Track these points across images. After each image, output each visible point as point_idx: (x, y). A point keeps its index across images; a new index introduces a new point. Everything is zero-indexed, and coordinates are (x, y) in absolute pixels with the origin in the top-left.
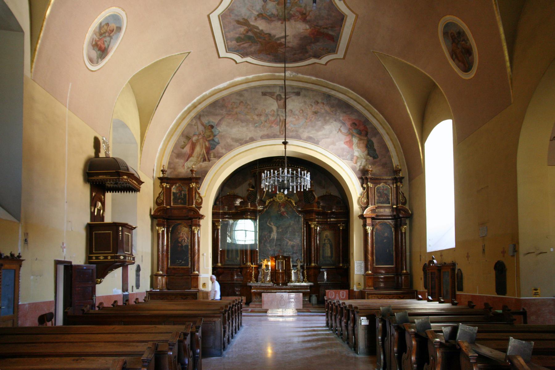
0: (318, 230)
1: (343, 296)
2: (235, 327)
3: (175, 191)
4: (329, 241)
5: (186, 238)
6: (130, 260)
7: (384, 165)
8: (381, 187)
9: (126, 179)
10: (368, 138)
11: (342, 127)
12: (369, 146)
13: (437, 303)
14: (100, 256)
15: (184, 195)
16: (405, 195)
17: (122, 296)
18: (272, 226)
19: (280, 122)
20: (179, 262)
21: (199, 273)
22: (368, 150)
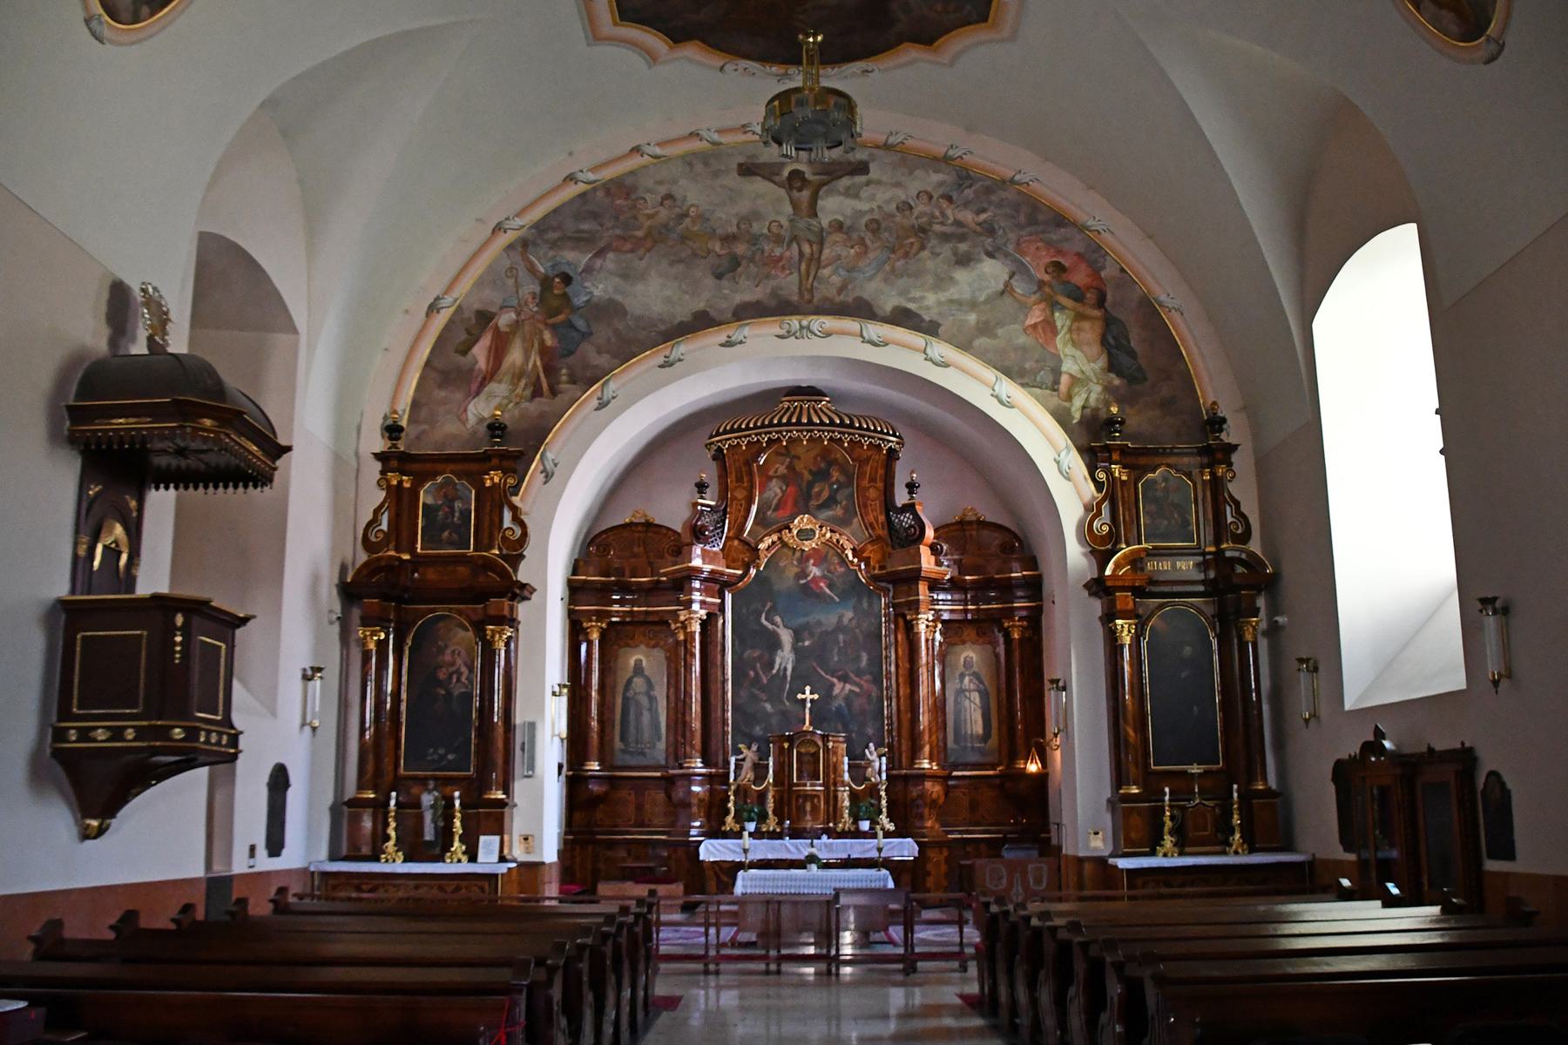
0: (937, 644)
1: (1038, 881)
2: (617, 1024)
3: (430, 501)
4: (975, 681)
5: (464, 669)
6: (219, 743)
7: (1166, 405)
8: (1160, 480)
9: (208, 431)
10: (1106, 310)
11: (1016, 277)
12: (1111, 341)
13: (1378, 908)
14: (98, 727)
15: (461, 512)
16: (1244, 509)
17: (203, 886)
18: (778, 627)
19: (800, 261)
20: (436, 757)
21: (508, 797)
22: (1110, 355)
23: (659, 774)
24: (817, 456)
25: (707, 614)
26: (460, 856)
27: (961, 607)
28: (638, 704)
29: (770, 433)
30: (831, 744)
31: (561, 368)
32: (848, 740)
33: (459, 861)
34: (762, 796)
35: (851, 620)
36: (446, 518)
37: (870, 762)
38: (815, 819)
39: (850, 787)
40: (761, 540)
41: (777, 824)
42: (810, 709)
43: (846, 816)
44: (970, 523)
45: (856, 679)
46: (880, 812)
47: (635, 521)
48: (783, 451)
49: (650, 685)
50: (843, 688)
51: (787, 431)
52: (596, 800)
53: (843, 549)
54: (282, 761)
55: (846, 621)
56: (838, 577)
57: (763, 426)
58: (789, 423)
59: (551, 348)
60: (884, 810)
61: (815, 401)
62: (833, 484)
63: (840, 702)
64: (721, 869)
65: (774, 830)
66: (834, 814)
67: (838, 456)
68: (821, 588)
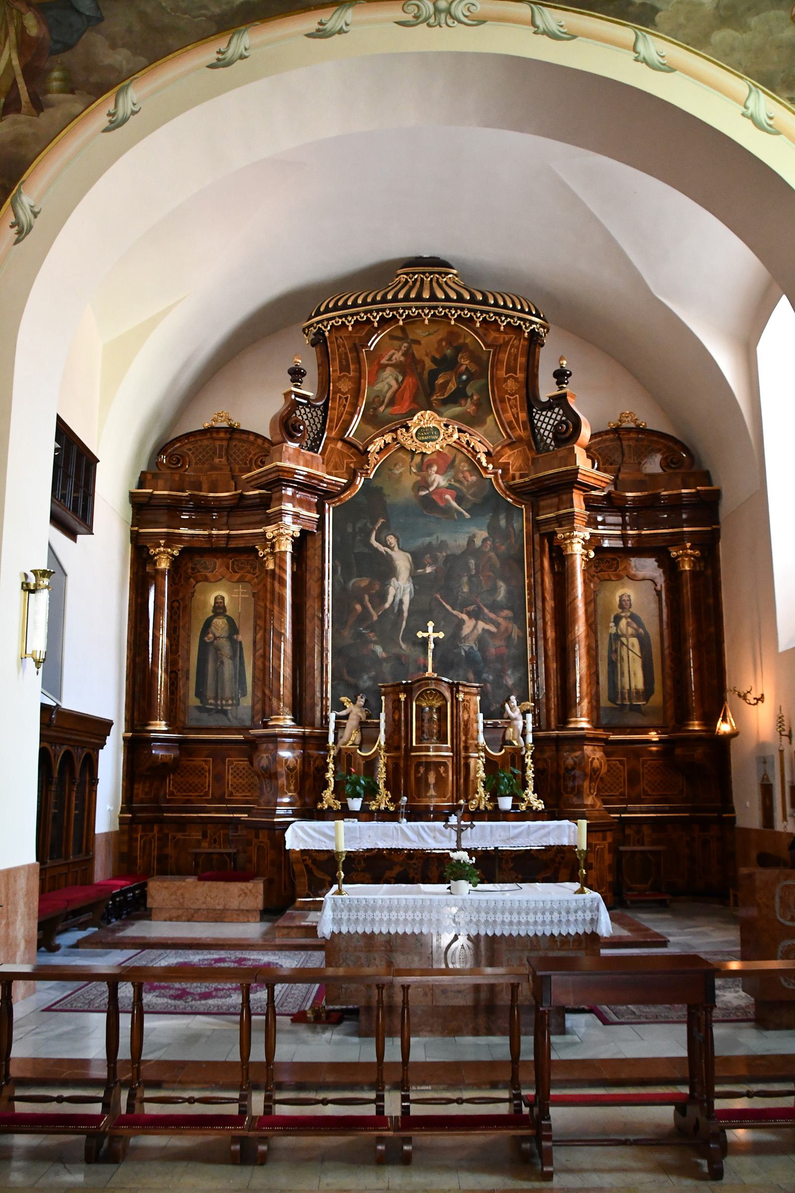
18: (392, 549)
23: (241, 737)
24: (441, 340)
25: (302, 531)
27: (619, 532)
28: (217, 650)
29: (384, 310)
30: (461, 697)
31: (51, 70)
32: (483, 693)
34: (370, 764)
35: (484, 541)
37: (510, 720)
38: (441, 794)
39: (485, 751)
40: (371, 442)
41: (390, 800)
42: (434, 651)
43: (481, 790)
44: (629, 430)
45: (492, 615)
46: (525, 786)
47: (218, 425)
48: (399, 334)
49: (233, 628)
50: (475, 627)
51: (404, 308)
52: (162, 770)
53: (475, 452)
55: (478, 542)
56: (469, 488)
57: (374, 302)
58: (406, 298)
59: (37, 39)
60: (531, 783)
61: (440, 273)
62: (463, 374)
63: (469, 645)
64: (314, 861)
65: (387, 809)
66: (465, 789)
67: (468, 341)
68: (447, 501)
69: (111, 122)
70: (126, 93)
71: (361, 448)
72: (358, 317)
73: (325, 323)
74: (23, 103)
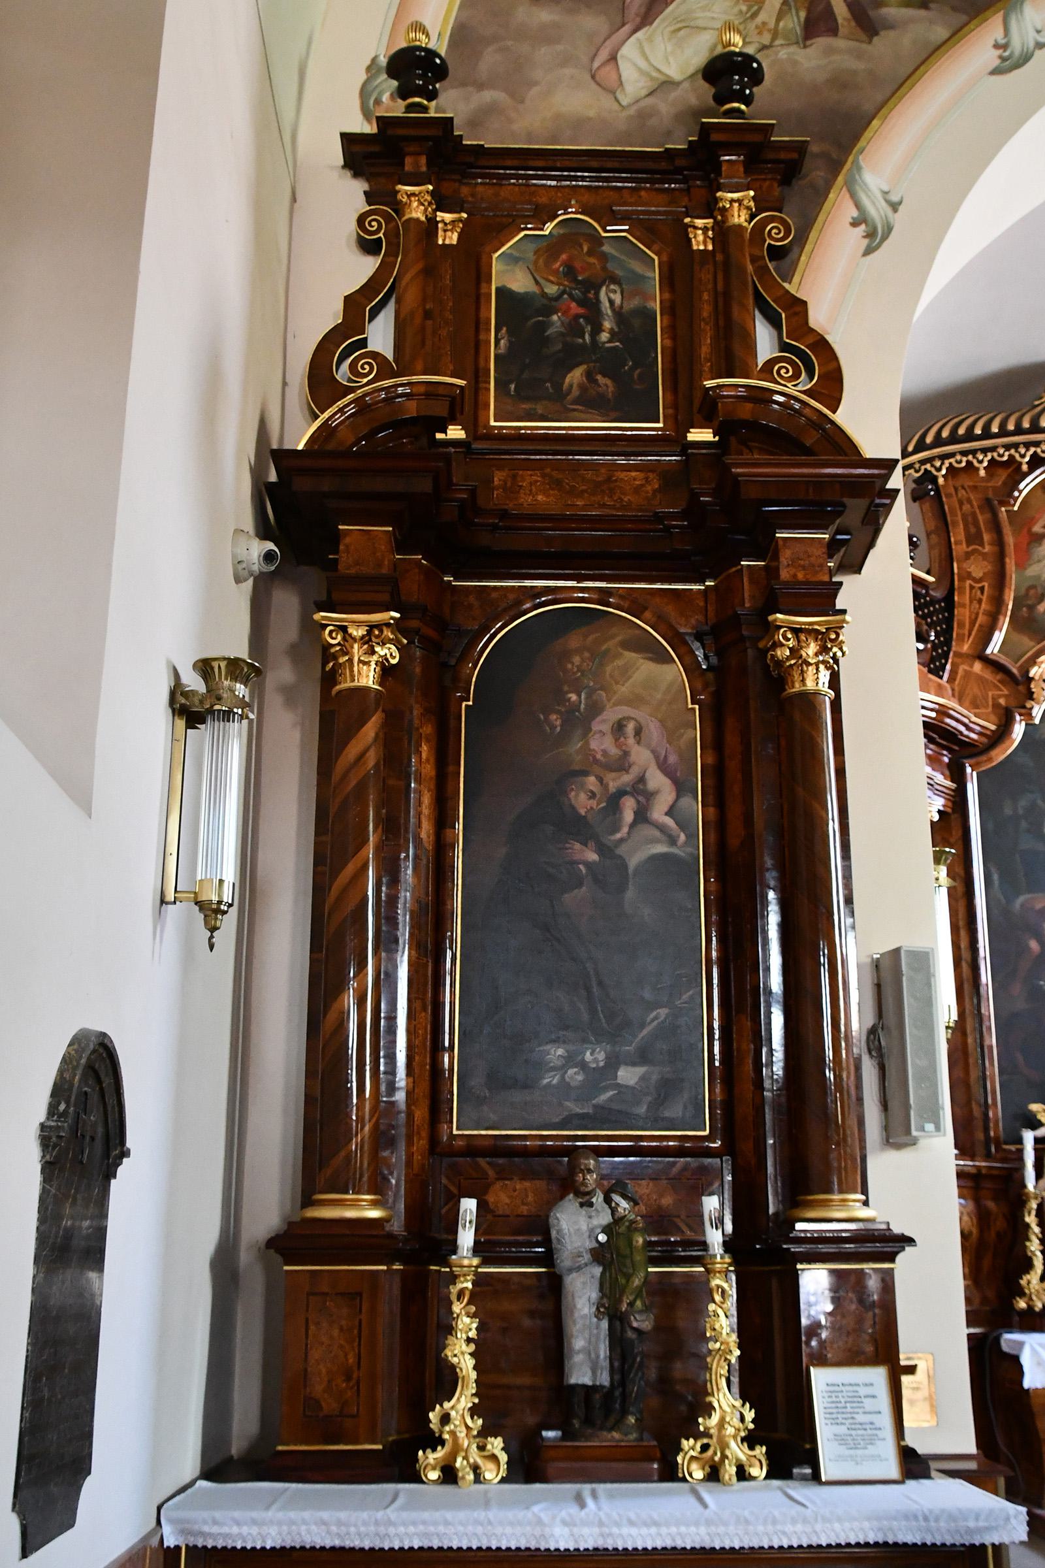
3: (520, 282)
26: (738, 1451)
33: (742, 1474)
36: (574, 328)
54: (97, 1025)
57: (1019, 431)
69: (1003, 59)
70: (1021, 12)
71: (1015, 671)
72: (995, 454)
73: (938, 464)
74: (840, 21)
